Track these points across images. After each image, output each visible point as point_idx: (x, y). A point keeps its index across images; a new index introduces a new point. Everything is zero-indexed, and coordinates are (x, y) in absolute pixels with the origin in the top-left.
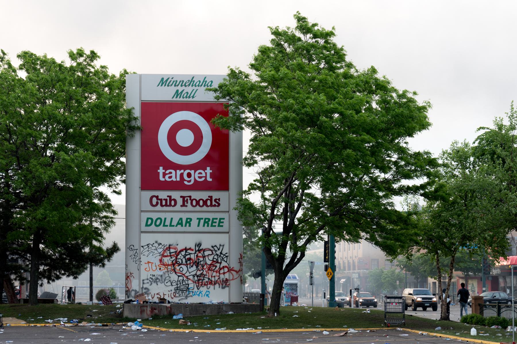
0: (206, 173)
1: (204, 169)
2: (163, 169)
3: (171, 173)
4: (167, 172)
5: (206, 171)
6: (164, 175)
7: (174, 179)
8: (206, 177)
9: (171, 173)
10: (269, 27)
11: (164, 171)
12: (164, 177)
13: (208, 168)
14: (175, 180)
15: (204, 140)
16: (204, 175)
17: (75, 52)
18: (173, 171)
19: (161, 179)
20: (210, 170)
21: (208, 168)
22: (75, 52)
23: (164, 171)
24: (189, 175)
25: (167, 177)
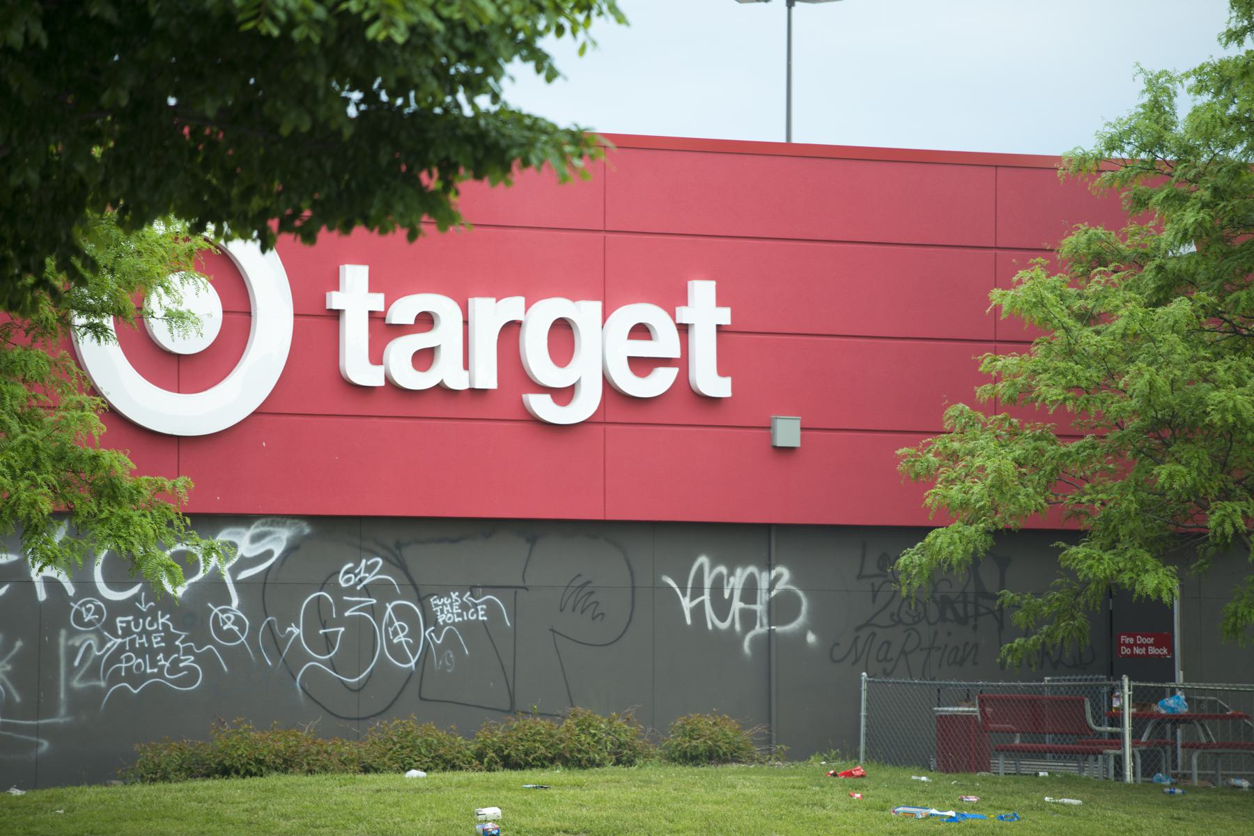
0: (684, 329)
1: (673, 298)
2: (374, 287)
3: (426, 321)
4: (404, 311)
5: (684, 315)
6: (382, 330)
7: (447, 371)
8: (682, 363)
9: (426, 321)
10: (628, 24)
11: (377, 302)
12: (376, 356)
13: (702, 291)
14: (459, 381)
15: (103, 585)
16: (665, 344)
17: (543, 76)
18: (443, 306)
19: (119, 619)
20: (721, 302)
21: (702, 291)
22: (543, 76)
23: (377, 302)
24: (562, 331)
25: (400, 352)
